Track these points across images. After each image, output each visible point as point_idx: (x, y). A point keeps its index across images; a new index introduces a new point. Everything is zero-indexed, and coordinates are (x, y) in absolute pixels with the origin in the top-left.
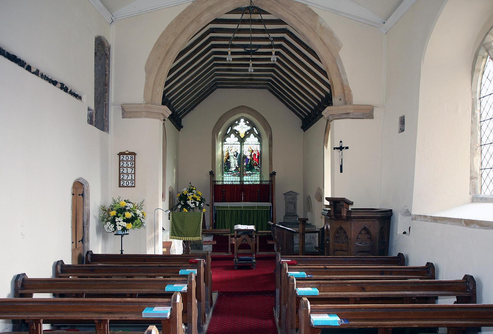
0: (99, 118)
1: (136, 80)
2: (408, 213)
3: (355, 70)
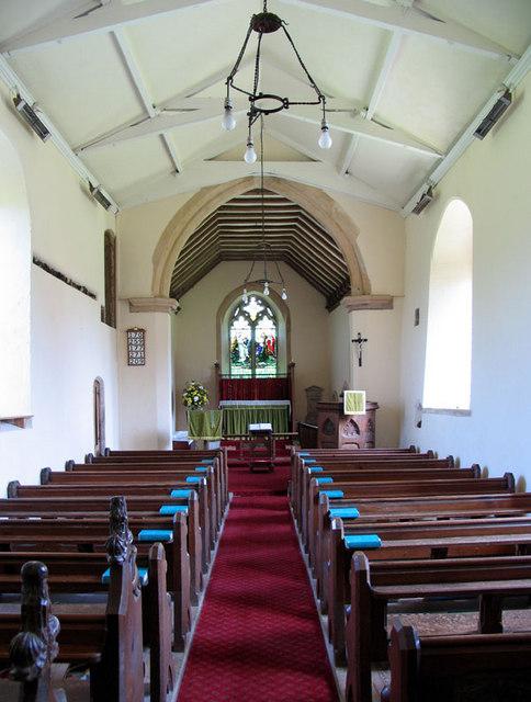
0: (109, 317)
1: (144, 275)
2: (420, 407)
3: (371, 261)
